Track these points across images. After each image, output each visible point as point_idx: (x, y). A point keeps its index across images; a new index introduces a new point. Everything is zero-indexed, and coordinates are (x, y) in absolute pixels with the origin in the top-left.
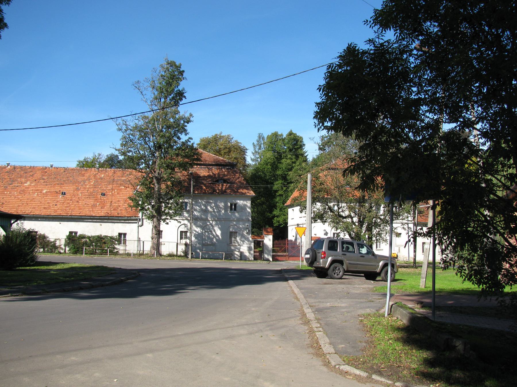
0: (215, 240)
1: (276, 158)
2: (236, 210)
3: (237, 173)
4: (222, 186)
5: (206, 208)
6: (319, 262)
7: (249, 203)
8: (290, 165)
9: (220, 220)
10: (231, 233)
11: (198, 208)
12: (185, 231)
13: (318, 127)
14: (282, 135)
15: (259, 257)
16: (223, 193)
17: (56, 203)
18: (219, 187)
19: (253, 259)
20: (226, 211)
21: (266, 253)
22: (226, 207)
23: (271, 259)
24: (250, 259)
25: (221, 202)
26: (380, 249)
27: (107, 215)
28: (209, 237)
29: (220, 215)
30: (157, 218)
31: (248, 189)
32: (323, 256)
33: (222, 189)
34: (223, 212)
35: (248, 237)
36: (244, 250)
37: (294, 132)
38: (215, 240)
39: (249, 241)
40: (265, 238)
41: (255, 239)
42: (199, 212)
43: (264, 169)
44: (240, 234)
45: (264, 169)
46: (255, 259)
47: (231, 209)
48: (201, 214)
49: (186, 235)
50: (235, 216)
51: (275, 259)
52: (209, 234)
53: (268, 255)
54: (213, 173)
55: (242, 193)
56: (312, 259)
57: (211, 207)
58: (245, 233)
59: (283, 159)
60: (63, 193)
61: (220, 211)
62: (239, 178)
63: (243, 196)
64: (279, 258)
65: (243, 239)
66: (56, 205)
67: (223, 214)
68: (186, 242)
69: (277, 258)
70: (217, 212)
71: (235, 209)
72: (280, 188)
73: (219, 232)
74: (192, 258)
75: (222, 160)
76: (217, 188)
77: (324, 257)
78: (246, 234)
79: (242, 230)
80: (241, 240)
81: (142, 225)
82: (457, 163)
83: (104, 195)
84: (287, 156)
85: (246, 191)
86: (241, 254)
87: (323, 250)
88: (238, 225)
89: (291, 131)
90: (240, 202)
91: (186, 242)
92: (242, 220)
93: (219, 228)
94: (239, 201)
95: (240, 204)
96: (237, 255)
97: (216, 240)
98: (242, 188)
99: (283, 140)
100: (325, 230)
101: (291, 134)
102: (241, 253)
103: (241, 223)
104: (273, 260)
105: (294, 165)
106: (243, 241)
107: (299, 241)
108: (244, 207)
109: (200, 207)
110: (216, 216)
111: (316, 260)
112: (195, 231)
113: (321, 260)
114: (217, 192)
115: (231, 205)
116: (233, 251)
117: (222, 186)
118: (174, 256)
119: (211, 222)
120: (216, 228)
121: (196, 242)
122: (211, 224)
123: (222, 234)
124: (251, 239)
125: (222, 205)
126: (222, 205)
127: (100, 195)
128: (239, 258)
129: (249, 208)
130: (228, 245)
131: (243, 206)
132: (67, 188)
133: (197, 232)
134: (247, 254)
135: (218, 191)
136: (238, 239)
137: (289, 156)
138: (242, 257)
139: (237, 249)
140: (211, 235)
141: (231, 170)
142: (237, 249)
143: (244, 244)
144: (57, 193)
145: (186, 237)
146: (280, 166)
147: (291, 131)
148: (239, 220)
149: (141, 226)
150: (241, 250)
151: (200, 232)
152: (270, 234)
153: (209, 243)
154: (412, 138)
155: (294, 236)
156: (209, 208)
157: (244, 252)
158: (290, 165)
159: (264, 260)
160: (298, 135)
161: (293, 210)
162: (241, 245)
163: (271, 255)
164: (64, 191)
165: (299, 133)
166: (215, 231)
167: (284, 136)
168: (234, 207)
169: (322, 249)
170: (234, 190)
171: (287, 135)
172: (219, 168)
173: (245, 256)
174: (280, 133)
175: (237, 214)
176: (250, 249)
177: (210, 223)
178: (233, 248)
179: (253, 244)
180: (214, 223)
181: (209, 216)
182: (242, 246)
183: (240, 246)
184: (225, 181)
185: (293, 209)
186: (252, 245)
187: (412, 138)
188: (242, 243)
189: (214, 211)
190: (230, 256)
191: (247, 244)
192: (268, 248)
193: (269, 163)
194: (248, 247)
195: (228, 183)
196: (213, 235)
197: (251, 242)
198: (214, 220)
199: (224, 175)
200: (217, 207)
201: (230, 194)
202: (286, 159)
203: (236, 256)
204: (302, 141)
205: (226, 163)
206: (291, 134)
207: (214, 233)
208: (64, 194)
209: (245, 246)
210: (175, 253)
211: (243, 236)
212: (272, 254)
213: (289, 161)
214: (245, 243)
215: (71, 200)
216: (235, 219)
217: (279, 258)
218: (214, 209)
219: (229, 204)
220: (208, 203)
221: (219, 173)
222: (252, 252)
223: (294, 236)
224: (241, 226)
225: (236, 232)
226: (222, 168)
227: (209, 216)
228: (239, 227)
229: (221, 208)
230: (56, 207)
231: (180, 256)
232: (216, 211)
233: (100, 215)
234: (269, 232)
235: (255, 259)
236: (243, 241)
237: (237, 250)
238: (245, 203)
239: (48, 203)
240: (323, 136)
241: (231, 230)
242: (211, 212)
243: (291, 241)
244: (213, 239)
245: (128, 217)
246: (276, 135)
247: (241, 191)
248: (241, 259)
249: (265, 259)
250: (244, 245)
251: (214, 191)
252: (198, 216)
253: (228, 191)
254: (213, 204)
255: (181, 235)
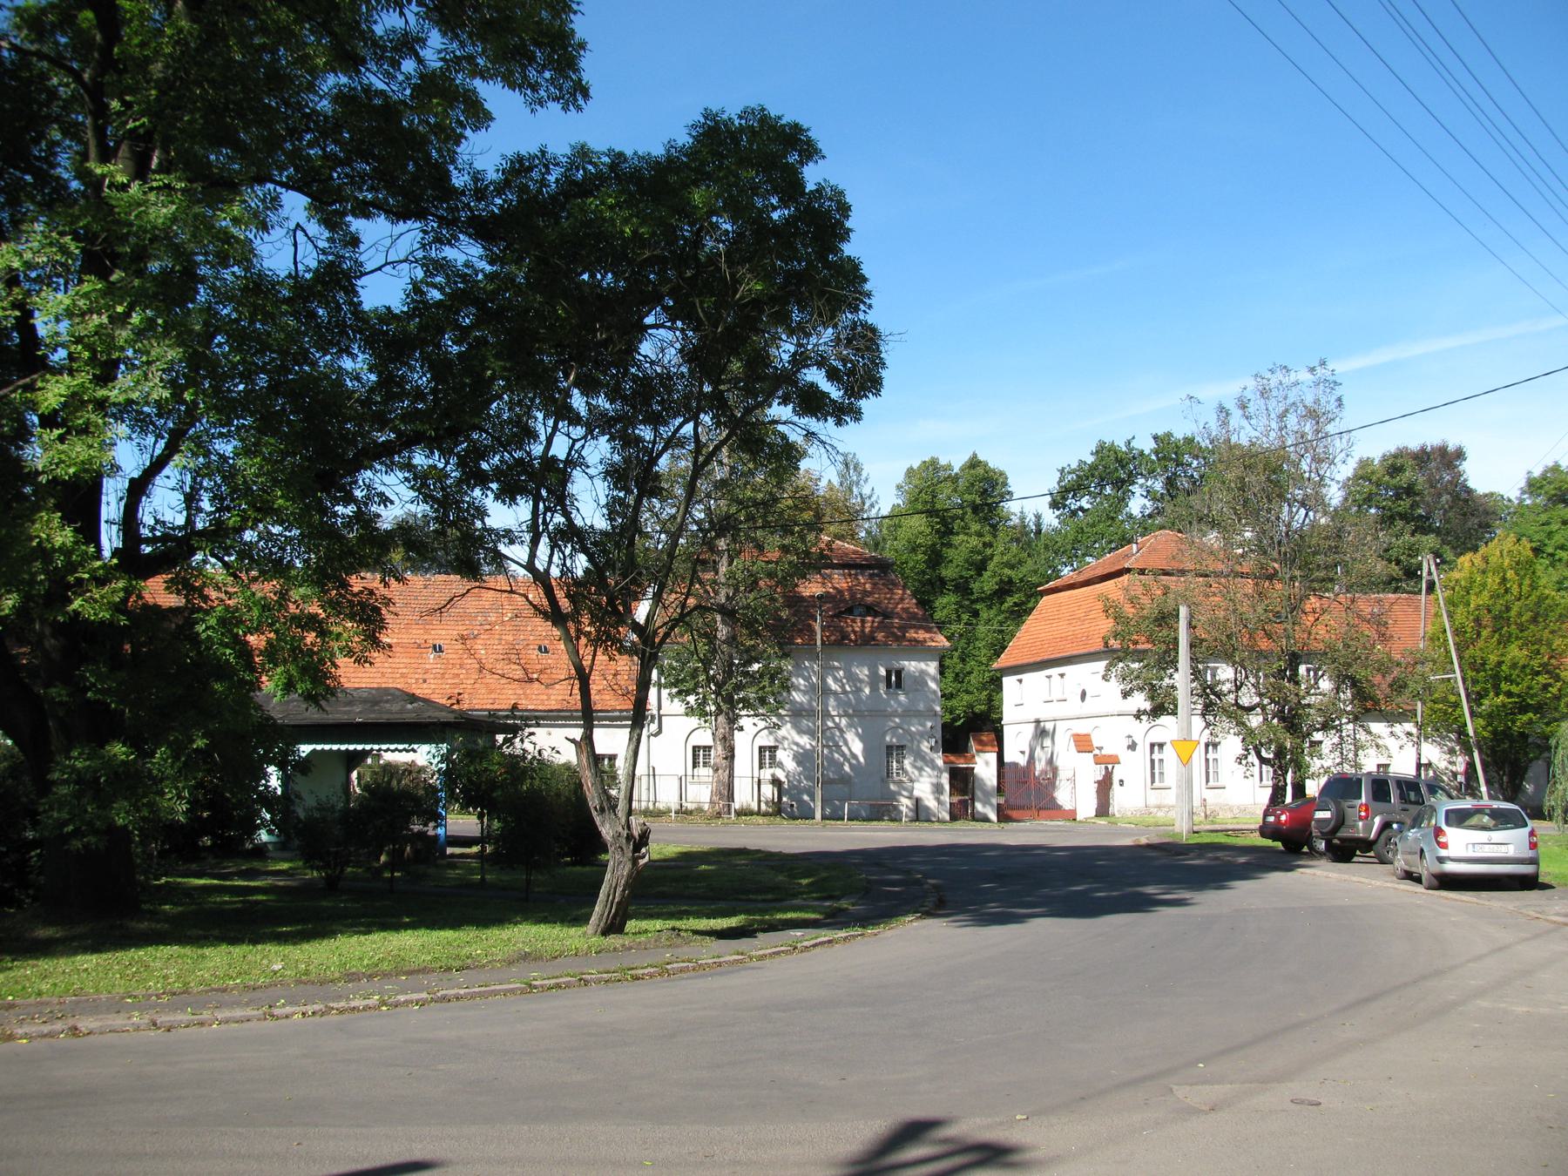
0: (847, 768)
1: (938, 531)
3: (896, 585)
4: (863, 622)
5: (824, 681)
6: (1354, 827)
7: (932, 668)
8: (979, 553)
9: (862, 715)
10: (890, 748)
11: (802, 681)
12: (770, 747)
14: (949, 467)
15: (961, 811)
16: (866, 641)
17: (425, 676)
18: (856, 625)
20: (874, 689)
21: (980, 801)
22: (874, 680)
25: (861, 665)
26: (1161, 785)
27: (564, 706)
28: (832, 761)
29: (858, 699)
30: (727, 714)
31: (928, 630)
32: (1363, 814)
33: (863, 631)
34: (867, 691)
37: (981, 457)
38: (847, 768)
39: (934, 767)
40: (977, 759)
41: (952, 763)
42: (805, 693)
43: (906, 563)
44: (912, 751)
45: (906, 563)
46: (954, 818)
47: (889, 685)
48: (811, 699)
49: (773, 757)
50: (899, 703)
51: (1003, 816)
52: (831, 752)
53: (986, 803)
54: (834, 588)
55: (915, 640)
56: (1337, 821)
57: (836, 680)
58: (925, 746)
59: (958, 534)
60: (435, 646)
61: (860, 690)
62: (902, 599)
63: (919, 650)
64: (1014, 814)
65: (919, 764)
66: (425, 681)
67: (867, 697)
68: (773, 775)
69: (1010, 812)
70: (852, 692)
71: (899, 685)
72: (954, 617)
73: (857, 747)
74: (824, 818)
75: (855, 552)
76: (850, 629)
77: (1366, 817)
78: (928, 751)
80: (915, 767)
81: (660, 731)
83: (546, 651)
84: (966, 527)
85: (927, 635)
87: (1363, 800)
89: (975, 455)
90: (912, 666)
91: (773, 775)
92: (919, 715)
93: (857, 734)
94: (906, 663)
97: (851, 765)
98: (914, 627)
99: (955, 479)
100: (1129, 737)
101: (974, 463)
102: (918, 802)
103: (915, 721)
105: (989, 551)
106: (920, 769)
107: (1040, 766)
108: (920, 679)
109: (807, 679)
110: (849, 704)
111: (1343, 823)
112: (797, 744)
113: (1361, 824)
114: (851, 640)
115: (889, 673)
116: (893, 796)
117: (863, 622)
118: (751, 813)
119: (837, 719)
120: (850, 736)
121: (799, 774)
122: (838, 727)
123: (866, 751)
124: (940, 762)
125: (863, 672)
126: (863, 672)
127: (537, 652)
129: (934, 679)
130: (883, 780)
132: (444, 632)
133: (802, 748)
134: (931, 803)
135: (853, 637)
136: (907, 763)
137: (975, 527)
138: (920, 813)
140: (836, 755)
141: (881, 579)
142: (905, 789)
143: (921, 775)
144: (419, 646)
145: (774, 763)
146: (950, 553)
147: (975, 455)
148: (909, 713)
149: (655, 735)
150: (916, 793)
151: (808, 747)
152: (989, 748)
153: (831, 775)
155: (1023, 753)
156: (830, 681)
158: (979, 553)
159: (974, 819)
160: (991, 465)
161: (1020, 681)
163: (991, 805)
164: (437, 643)
165: (995, 461)
166: (846, 743)
167: (956, 470)
168: (896, 680)
169: (1360, 798)
170: (894, 634)
171: (962, 469)
172: (850, 575)
173: (927, 808)
174: (943, 462)
175: (902, 698)
176: (938, 789)
177: (834, 721)
178: (892, 787)
180: (844, 722)
181: (832, 702)
184: (870, 610)
185: (1019, 677)
186: (945, 780)
188: (916, 773)
189: (845, 692)
190: (883, 811)
193: (920, 545)
194: (933, 784)
195: (876, 614)
196: (843, 755)
197: (941, 771)
198: (846, 715)
199: (865, 592)
200: (852, 677)
201: (886, 644)
202: (967, 534)
204: (1005, 484)
205: (866, 559)
206: (974, 463)
207: (844, 749)
208: (438, 649)
210: (755, 807)
211: (919, 755)
212: (994, 801)
213: (974, 542)
215: (461, 666)
217: (1014, 814)
218: (843, 686)
219: (883, 672)
220: (827, 670)
221: (850, 589)
222: (946, 798)
223: (1023, 753)
225: (902, 747)
226: (856, 575)
227: (832, 702)
228: (908, 732)
229: (861, 681)
230: (425, 686)
231: (766, 814)
232: (848, 688)
233: (549, 708)
235: (954, 818)
236: (920, 769)
237: (905, 793)
238: (922, 665)
239: (403, 675)
240: (1063, 469)
241: (888, 739)
242: (835, 693)
243: (1015, 765)
244: (843, 764)
245: (621, 711)
246: (932, 465)
247: (911, 634)
248: (917, 819)
250: (922, 779)
251: (845, 636)
252: (801, 704)
253: (880, 636)
254: (841, 673)
255: (694, 755)
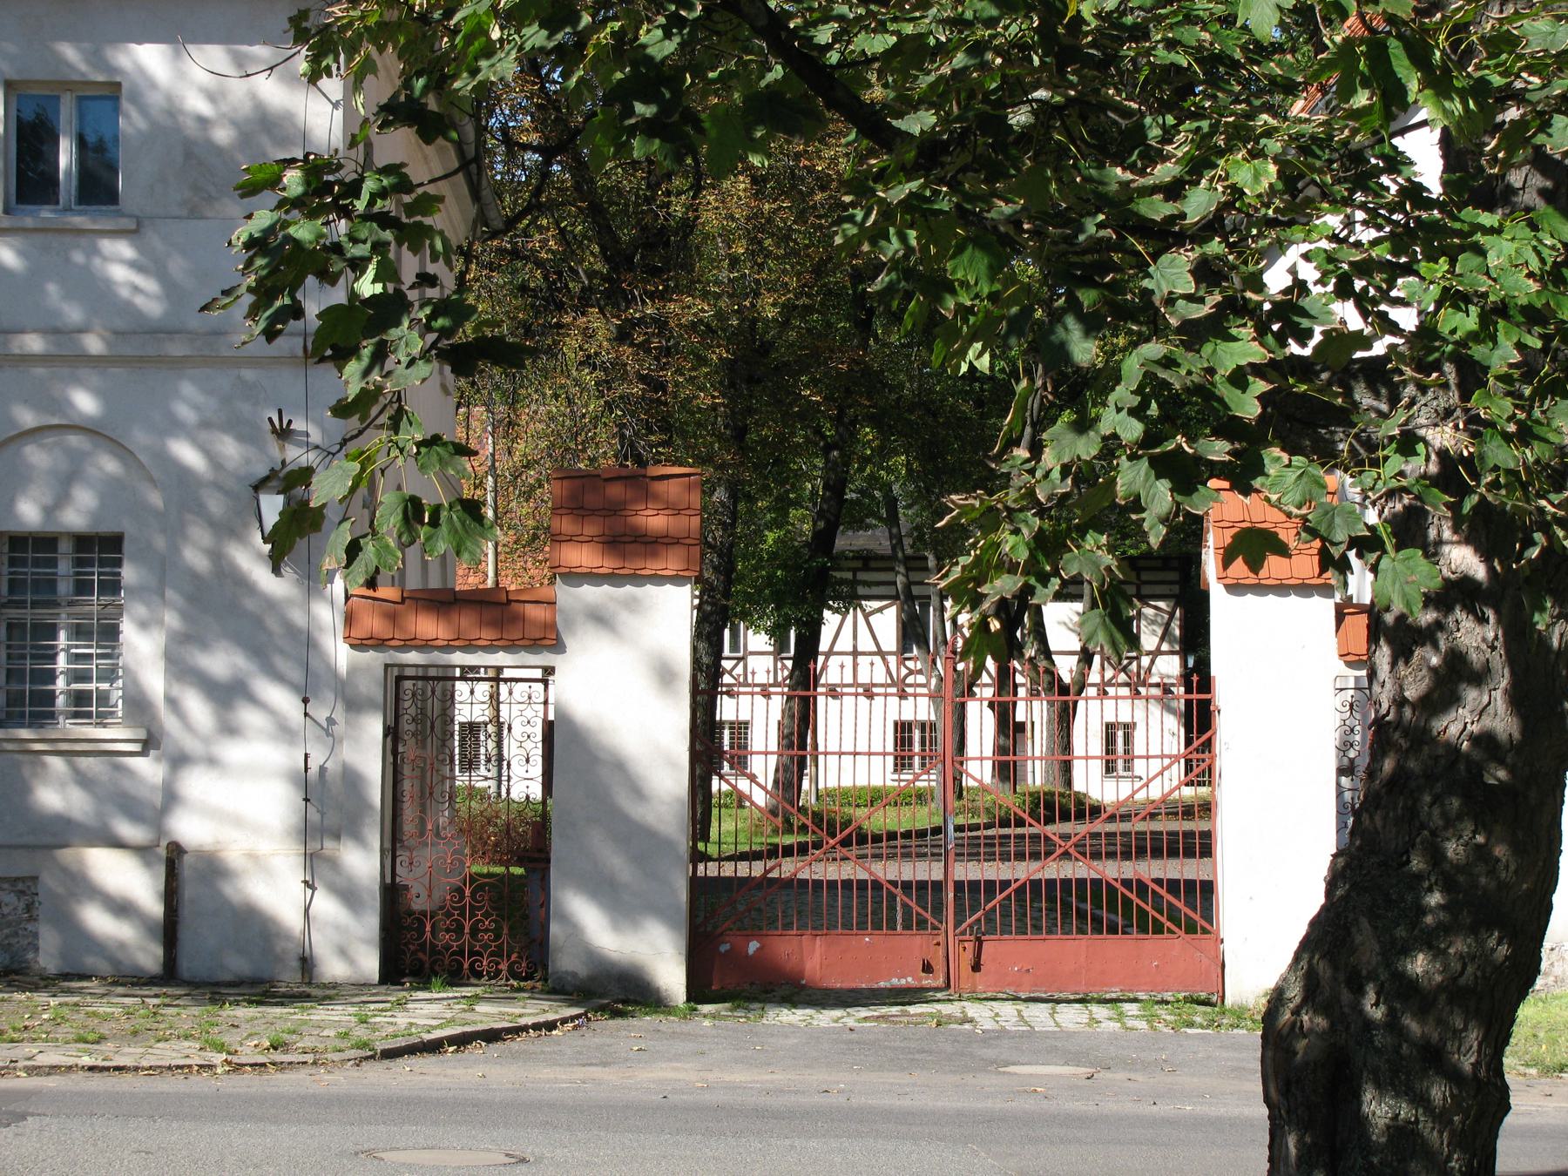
2: (111, 197)
13: (428, 762)
19: (370, 963)
23: (671, 976)
24: (333, 968)
35: (298, 617)
36: (237, 821)
50: (97, 293)
65: (220, 662)
79: (200, 510)
82: (185, 412)
86: (171, 895)
88: (139, 438)
95: (173, 111)
96: (122, 908)
104: (699, 991)
128: (150, 957)
131: (223, 135)
139: (132, 808)
142: (132, 808)
143: (229, 729)
150: (189, 829)
154: (1057, 98)
157: (234, 856)
162: (190, 744)
179: (374, 727)
182: (212, 762)
183: (179, 761)
187: (1057, 98)
188: (198, 708)
191: (285, 732)
192: (638, 791)
203: (98, 920)
209: (251, 771)
214: (249, 717)
216: (94, 344)
224: (187, 454)
234: (652, 544)
249: (566, 962)
250: (233, 752)
